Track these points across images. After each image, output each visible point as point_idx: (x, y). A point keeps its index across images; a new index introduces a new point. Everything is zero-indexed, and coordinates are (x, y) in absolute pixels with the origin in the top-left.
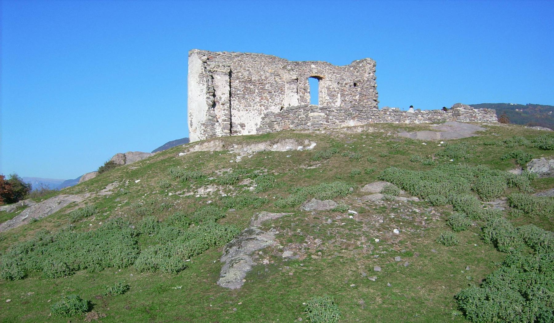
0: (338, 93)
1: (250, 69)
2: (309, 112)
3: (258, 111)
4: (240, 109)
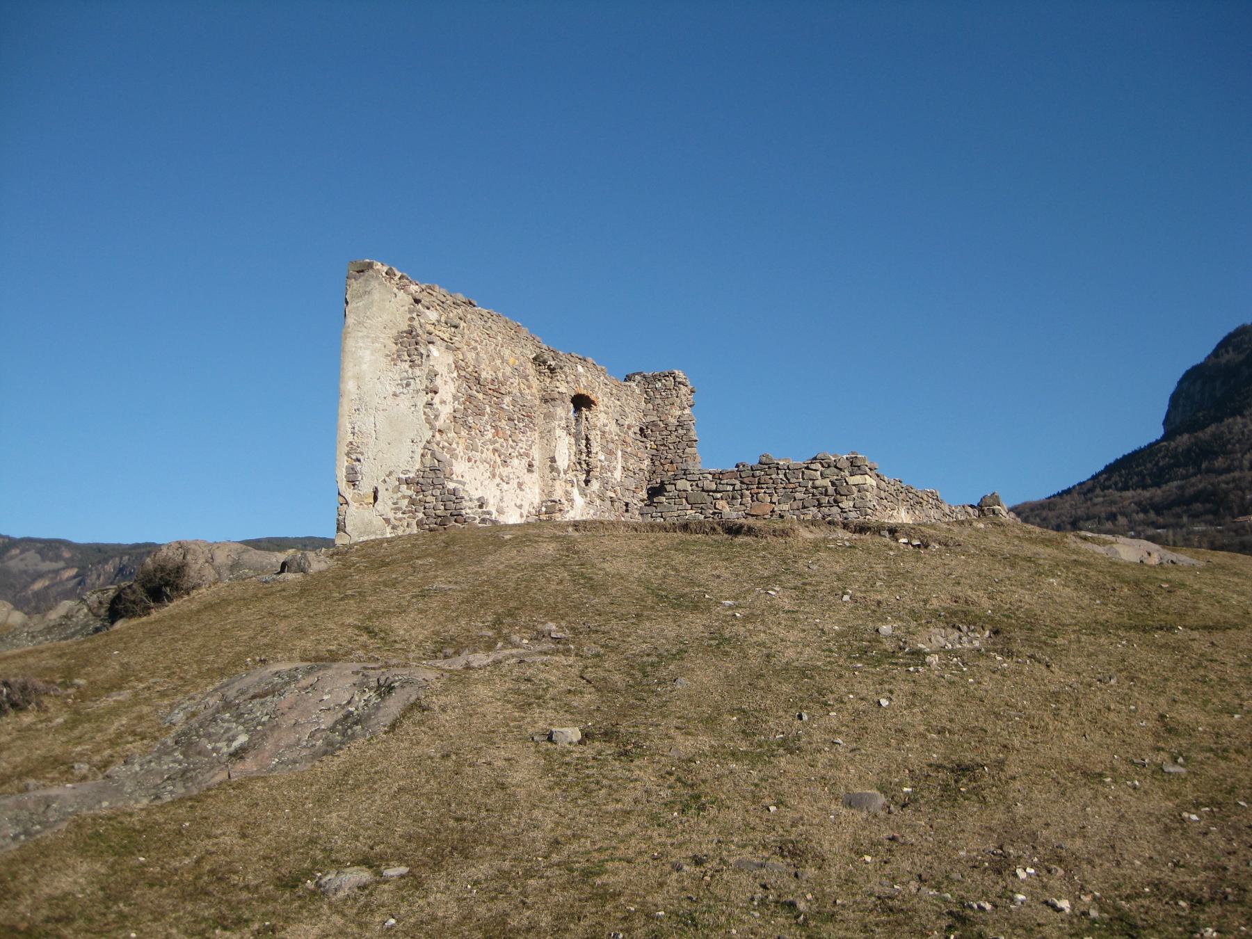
1: (479, 347)
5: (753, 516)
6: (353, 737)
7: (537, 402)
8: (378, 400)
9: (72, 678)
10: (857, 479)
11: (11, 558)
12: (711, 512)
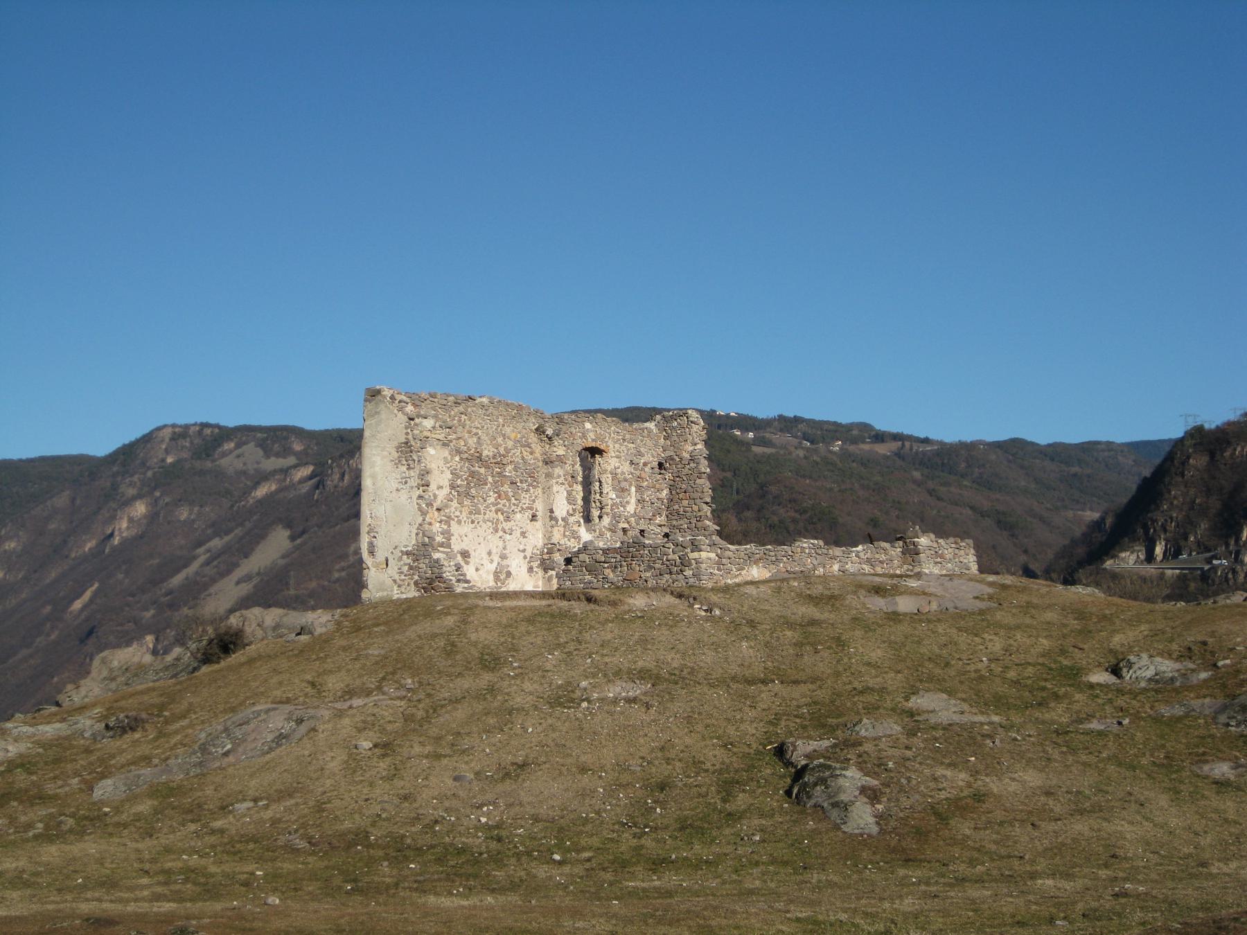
1: (480, 432)
4: (461, 518)
6: (281, 745)
7: (540, 464)
9: (162, 712)
10: (696, 555)
11: (224, 455)
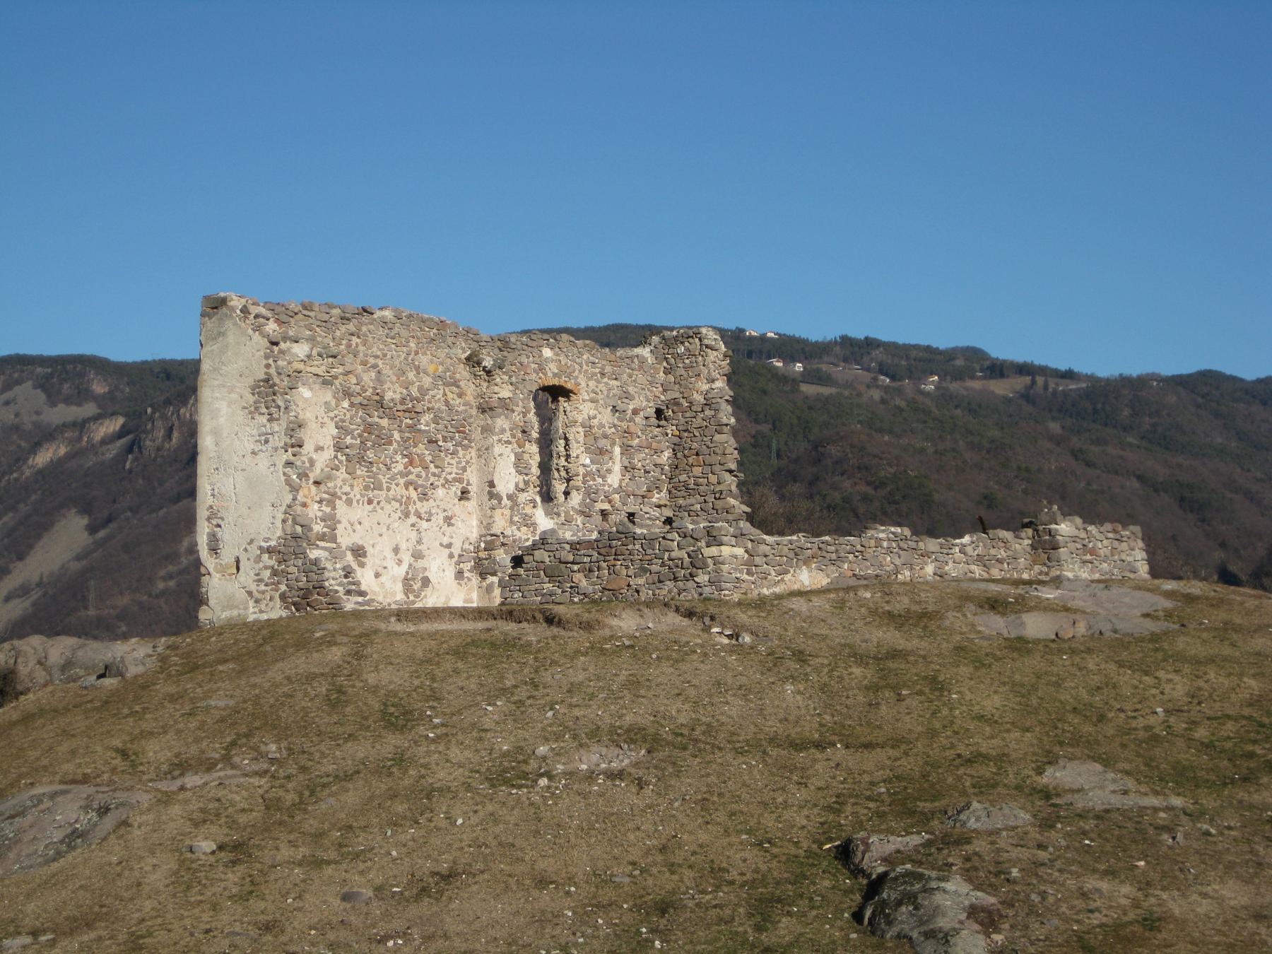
0: (613, 444)
1: (380, 363)
2: (703, 544)
3: (401, 505)
4: (351, 496)
5: (609, 590)
6: (74, 848)
7: (474, 412)
8: (236, 459)
10: (714, 551)
12: (569, 585)
